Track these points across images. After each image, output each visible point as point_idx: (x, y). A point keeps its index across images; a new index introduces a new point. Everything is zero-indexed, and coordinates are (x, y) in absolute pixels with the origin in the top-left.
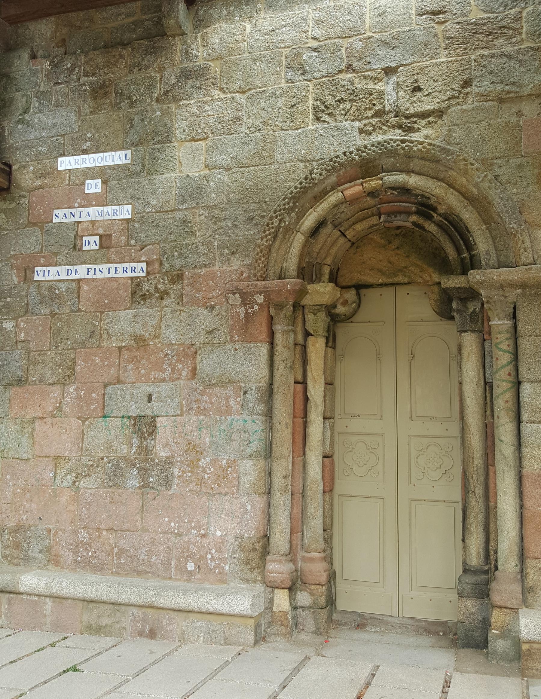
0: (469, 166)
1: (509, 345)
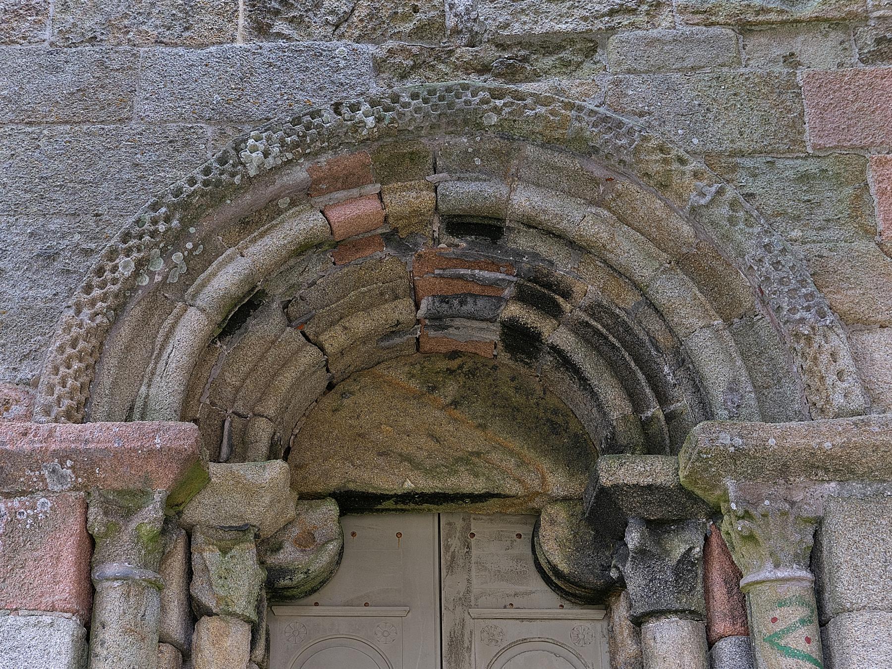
0: (675, 166)
1: (808, 640)
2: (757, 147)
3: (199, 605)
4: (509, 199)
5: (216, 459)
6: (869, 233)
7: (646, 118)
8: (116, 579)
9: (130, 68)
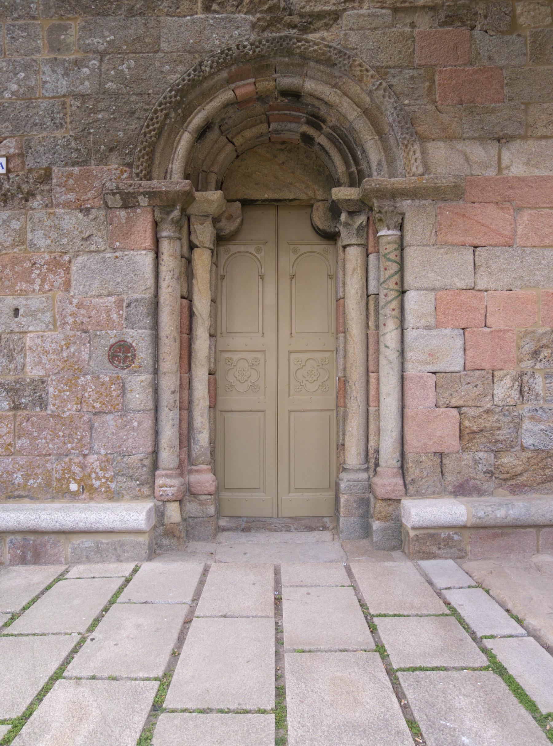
0: (365, 73)
1: (396, 256)
2: (397, 64)
3: (193, 243)
4: (303, 85)
5: (197, 190)
6: (434, 102)
7: (355, 51)
8: (166, 237)
9: (157, 27)
